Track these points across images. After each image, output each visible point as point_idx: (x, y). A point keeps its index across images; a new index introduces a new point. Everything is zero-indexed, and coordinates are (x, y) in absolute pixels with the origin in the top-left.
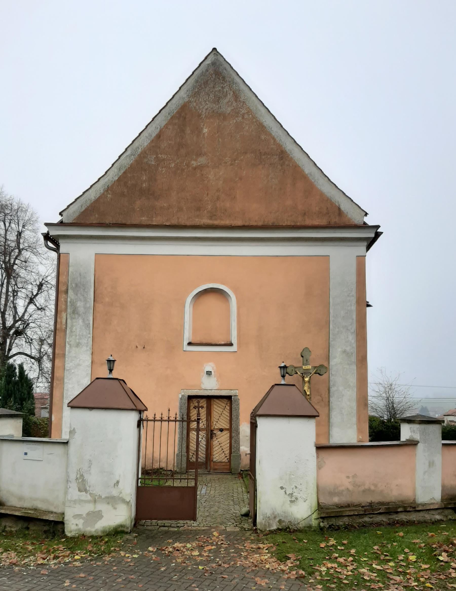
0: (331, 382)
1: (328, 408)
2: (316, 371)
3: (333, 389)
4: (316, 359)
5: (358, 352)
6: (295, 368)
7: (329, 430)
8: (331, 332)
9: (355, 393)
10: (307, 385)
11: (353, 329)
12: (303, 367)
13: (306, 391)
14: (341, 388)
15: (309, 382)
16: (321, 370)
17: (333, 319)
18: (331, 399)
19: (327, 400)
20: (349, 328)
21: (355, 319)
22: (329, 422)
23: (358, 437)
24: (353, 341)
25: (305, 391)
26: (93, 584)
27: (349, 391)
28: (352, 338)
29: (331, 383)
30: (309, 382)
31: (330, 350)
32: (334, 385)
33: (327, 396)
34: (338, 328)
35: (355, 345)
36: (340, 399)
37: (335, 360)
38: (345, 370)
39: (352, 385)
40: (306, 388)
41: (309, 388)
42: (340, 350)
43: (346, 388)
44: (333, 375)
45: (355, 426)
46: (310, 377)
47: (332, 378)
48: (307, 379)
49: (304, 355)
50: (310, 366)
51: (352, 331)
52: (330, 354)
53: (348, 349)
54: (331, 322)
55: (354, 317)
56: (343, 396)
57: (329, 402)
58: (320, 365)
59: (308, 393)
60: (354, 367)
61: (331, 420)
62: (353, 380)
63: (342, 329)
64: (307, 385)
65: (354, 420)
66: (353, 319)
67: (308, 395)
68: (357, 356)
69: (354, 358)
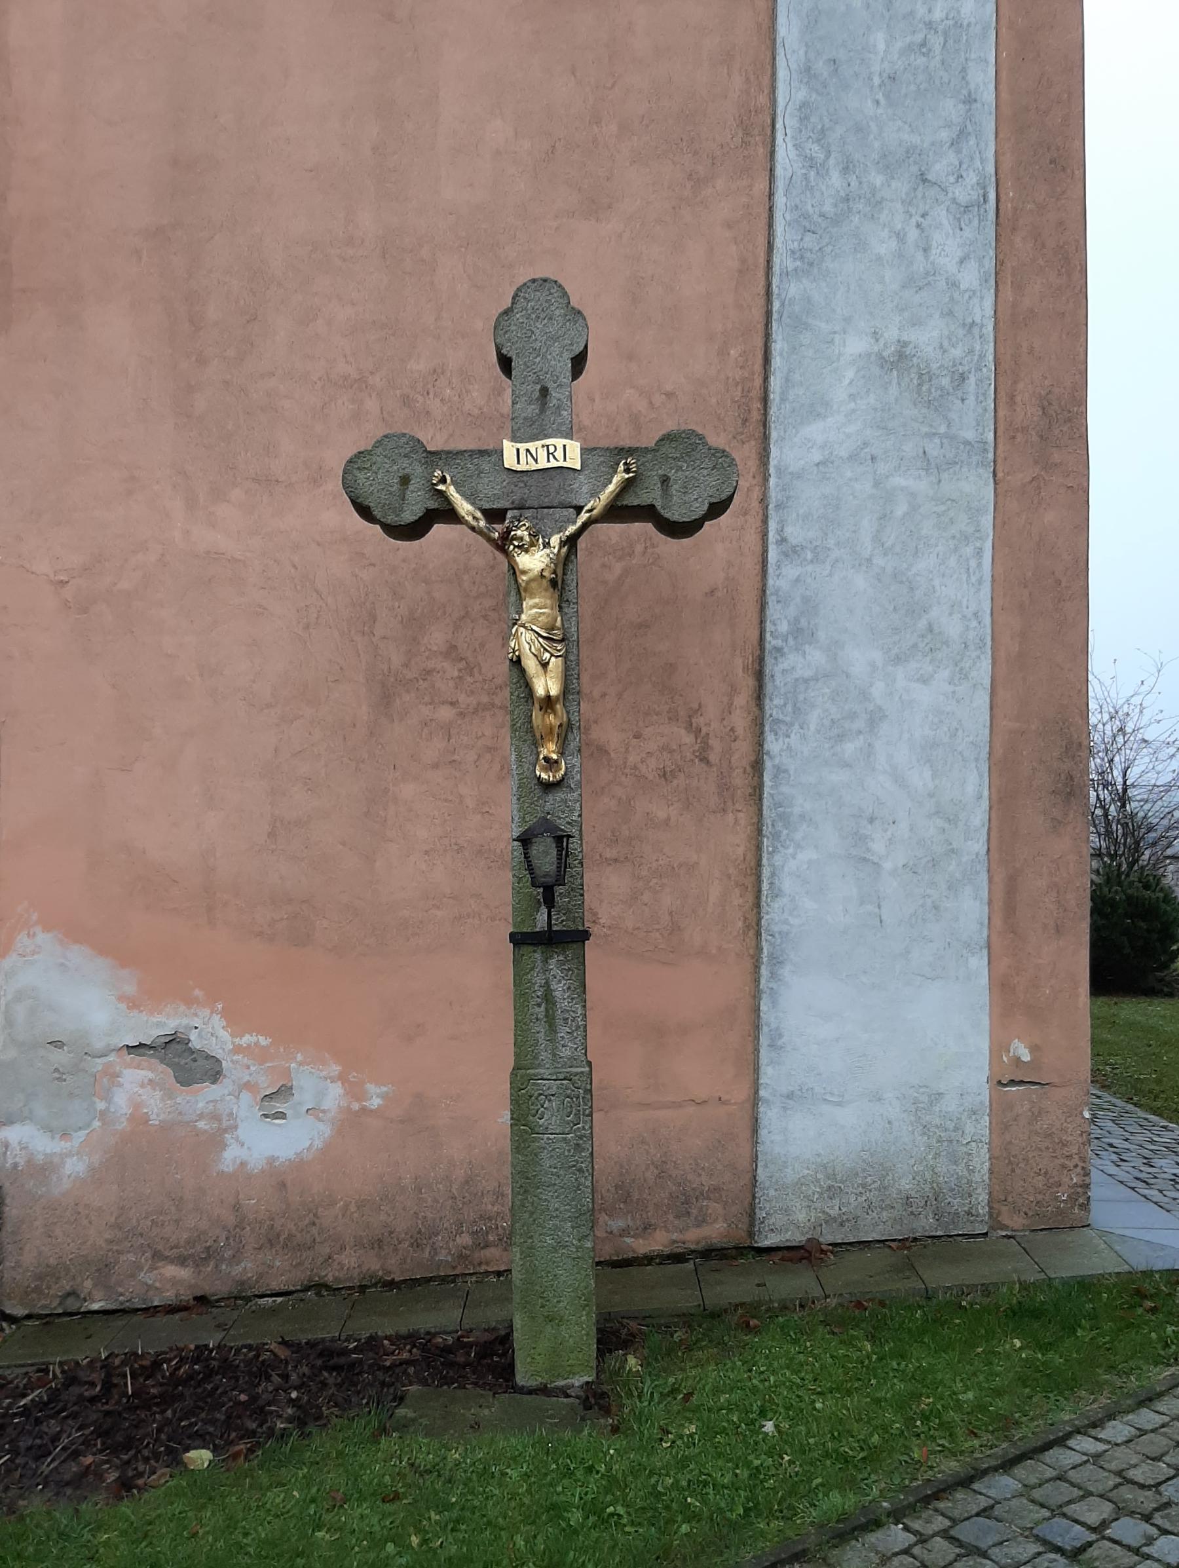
0: (774, 610)
1: (744, 818)
2: (627, 486)
3: (789, 668)
4: (637, 384)
5: (1006, 371)
6: (433, 457)
7: (756, 995)
8: (780, 200)
9: (982, 699)
10: (536, 608)
11: (971, 178)
12: (509, 449)
13: (530, 664)
14: (860, 658)
15: (553, 583)
16: (674, 493)
17: (801, 95)
18: (773, 744)
19: (742, 750)
20: (940, 169)
21: (988, 95)
22: (755, 926)
23: (998, 1048)
24: (970, 277)
25: (517, 662)
26: (906, 736)
27: (925, 681)
28: (961, 255)
29: (779, 620)
30: (553, 583)
31: (778, 346)
32: (801, 634)
33: (740, 721)
34: (847, 169)
35: (983, 309)
36: (850, 748)
37: (815, 431)
38: (901, 509)
39: (953, 628)
40: (526, 642)
41: (560, 638)
42: (856, 345)
43: (898, 660)
44: (792, 552)
45: (979, 963)
46: (571, 542)
47: (782, 578)
48: (534, 562)
49: (536, 350)
50: (574, 449)
51: (964, 192)
52: (775, 383)
53: (926, 339)
54: (786, 122)
55: (983, 80)
56: (876, 718)
57: (757, 766)
58: (668, 438)
59: (546, 684)
60: (977, 486)
61: (774, 914)
62: (962, 591)
63: (878, 180)
64: (536, 608)
65: (971, 910)
66: (970, 100)
67: (548, 703)
68: (1005, 396)
69: (973, 416)
